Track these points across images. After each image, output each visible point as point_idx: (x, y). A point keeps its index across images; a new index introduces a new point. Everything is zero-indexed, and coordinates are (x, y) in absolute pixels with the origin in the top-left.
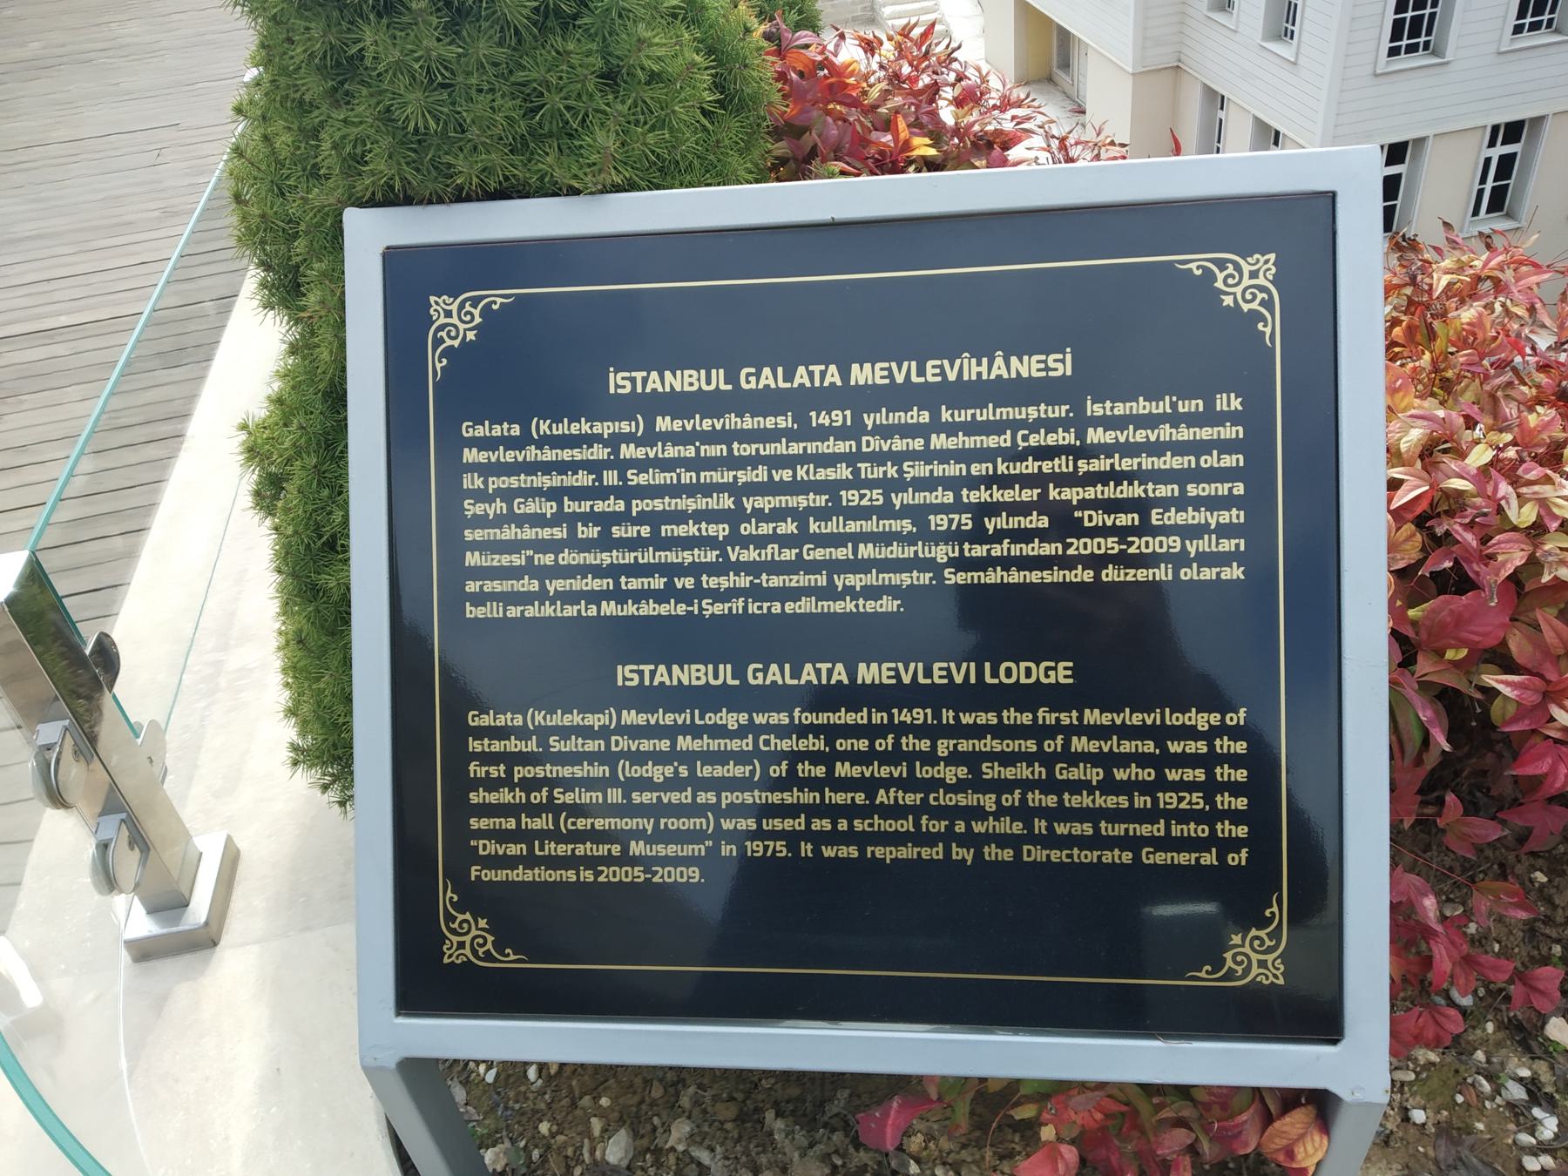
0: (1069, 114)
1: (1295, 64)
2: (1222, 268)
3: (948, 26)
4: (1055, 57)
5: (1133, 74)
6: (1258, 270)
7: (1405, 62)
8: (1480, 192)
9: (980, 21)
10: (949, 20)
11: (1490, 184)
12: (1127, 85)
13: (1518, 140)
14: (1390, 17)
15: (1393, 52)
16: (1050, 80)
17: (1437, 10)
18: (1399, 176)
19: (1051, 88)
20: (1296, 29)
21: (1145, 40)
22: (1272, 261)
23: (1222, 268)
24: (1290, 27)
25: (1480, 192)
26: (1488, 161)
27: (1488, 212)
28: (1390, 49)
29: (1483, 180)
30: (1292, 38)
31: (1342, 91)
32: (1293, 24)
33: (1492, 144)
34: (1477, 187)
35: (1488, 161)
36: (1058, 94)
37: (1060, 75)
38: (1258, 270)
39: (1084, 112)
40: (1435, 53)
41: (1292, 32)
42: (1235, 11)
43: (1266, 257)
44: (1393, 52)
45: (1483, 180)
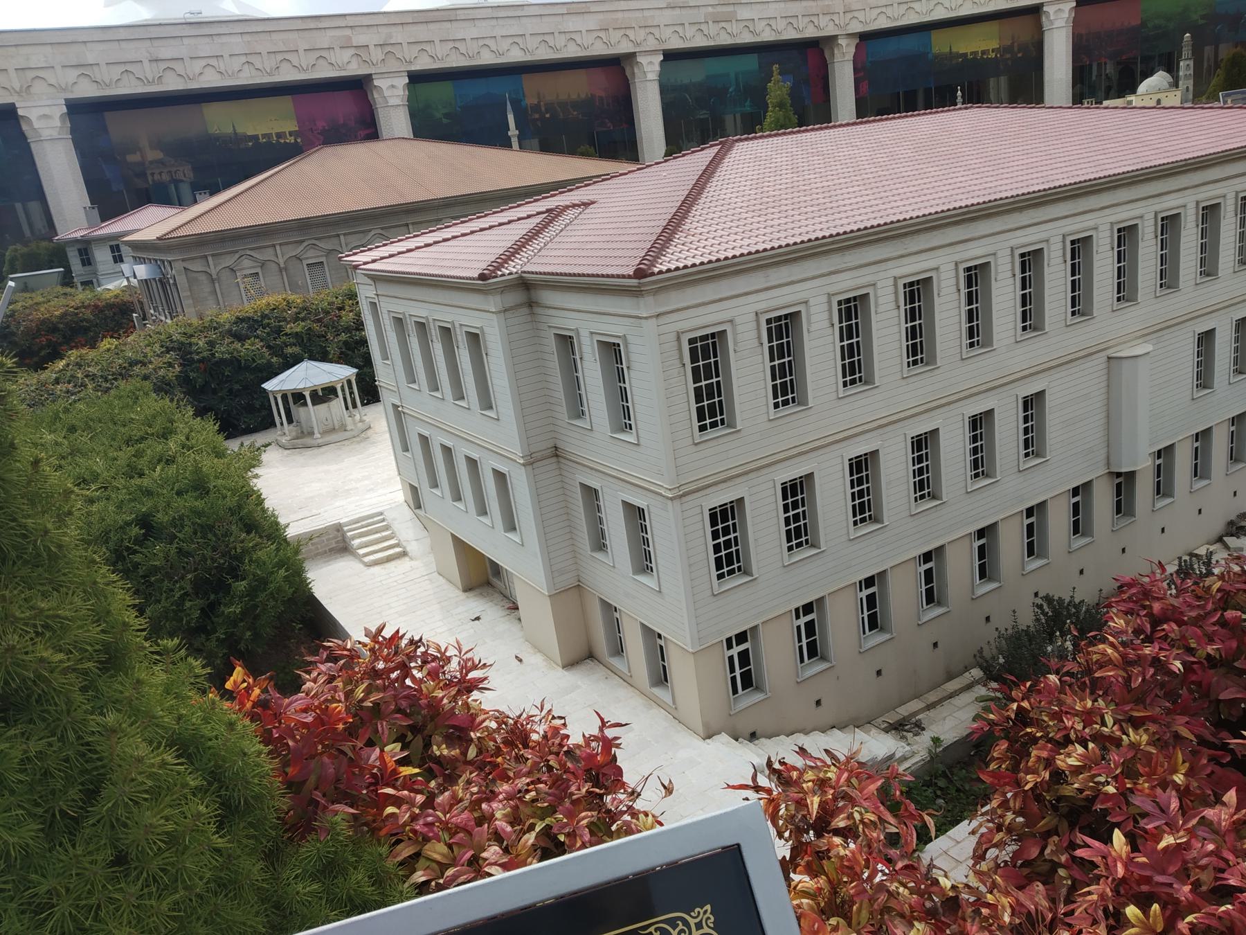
0: (508, 612)
1: (638, 445)
2: (675, 927)
3: (404, 548)
4: (489, 570)
5: (524, 465)
6: (701, 920)
7: (711, 433)
8: (801, 648)
9: (428, 541)
10: (404, 544)
11: (804, 642)
12: (548, 602)
13: (813, 612)
14: (694, 406)
15: (720, 577)
16: (488, 584)
17: (739, 547)
18: (747, 650)
19: (490, 590)
20: (632, 422)
21: (552, 571)
22: (709, 911)
23: (675, 927)
24: (628, 422)
25: (801, 648)
26: (799, 628)
27: (809, 659)
28: (714, 545)
29: (800, 640)
30: (631, 429)
31: (690, 566)
32: (630, 419)
33: (798, 617)
34: (797, 645)
35: (799, 628)
36: (496, 595)
37: (495, 581)
38: (701, 920)
39: (517, 609)
40: (729, 426)
41: (630, 425)
42: (609, 550)
43: (705, 908)
44: (720, 577)
45: (800, 640)
